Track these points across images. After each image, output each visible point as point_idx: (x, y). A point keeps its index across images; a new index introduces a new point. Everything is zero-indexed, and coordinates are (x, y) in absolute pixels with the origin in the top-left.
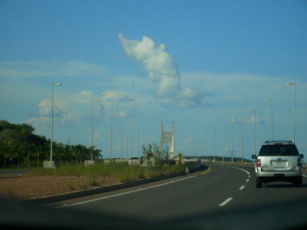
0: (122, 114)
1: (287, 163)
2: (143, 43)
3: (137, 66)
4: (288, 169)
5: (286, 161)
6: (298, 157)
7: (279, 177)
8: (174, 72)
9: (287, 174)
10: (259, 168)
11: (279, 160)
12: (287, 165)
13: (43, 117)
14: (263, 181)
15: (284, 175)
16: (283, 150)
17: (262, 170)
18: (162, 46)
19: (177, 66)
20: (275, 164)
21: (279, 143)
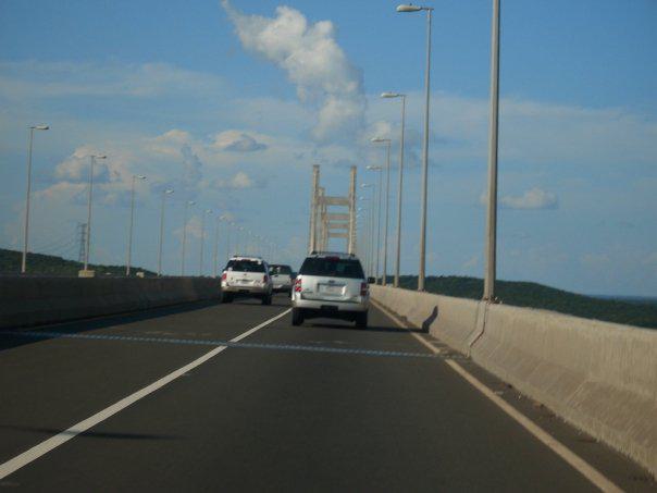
0: (241, 179)
1: (344, 290)
2: (282, 21)
3: (270, 73)
4: (346, 298)
5: (342, 285)
6: (361, 281)
7: (329, 312)
8: (351, 87)
9: (341, 306)
10: (298, 295)
11: (331, 284)
12: (344, 292)
13: (65, 185)
14: (302, 315)
15: (336, 308)
16: (341, 268)
17: (302, 298)
18: (325, 27)
19: (359, 73)
20: (324, 289)
21: (334, 255)
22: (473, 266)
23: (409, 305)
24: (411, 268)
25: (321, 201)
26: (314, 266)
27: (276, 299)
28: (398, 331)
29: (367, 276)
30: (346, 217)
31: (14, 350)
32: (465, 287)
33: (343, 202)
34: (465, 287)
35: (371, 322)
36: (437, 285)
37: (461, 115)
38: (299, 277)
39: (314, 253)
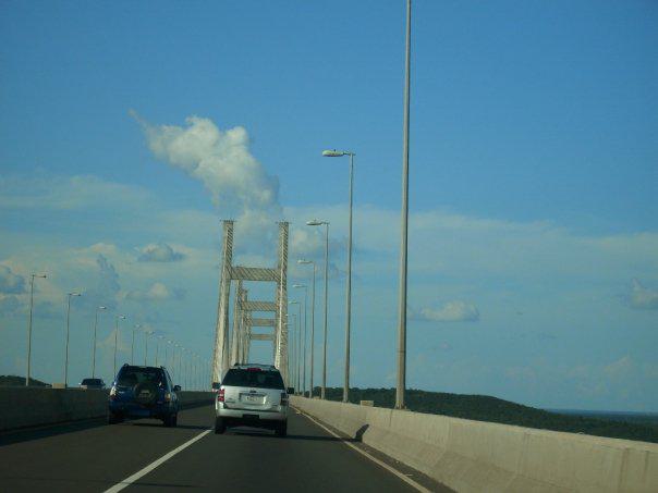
0: (159, 290)
2: (194, 131)
3: (183, 181)
4: (266, 408)
8: (266, 195)
9: (262, 415)
10: (221, 404)
11: (253, 394)
14: (225, 424)
16: (261, 379)
17: (225, 407)
18: (237, 135)
20: (245, 399)
22: (389, 381)
23: (340, 417)
24: (336, 381)
25: (235, 274)
26: (234, 377)
27: (183, 417)
28: (321, 437)
29: (286, 386)
30: (273, 307)
31: (13, 445)
32: (383, 398)
33: (269, 276)
34: (383, 398)
35: (289, 432)
36: (356, 396)
37: (378, 226)
38: (222, 388)
39: (236, 364)
